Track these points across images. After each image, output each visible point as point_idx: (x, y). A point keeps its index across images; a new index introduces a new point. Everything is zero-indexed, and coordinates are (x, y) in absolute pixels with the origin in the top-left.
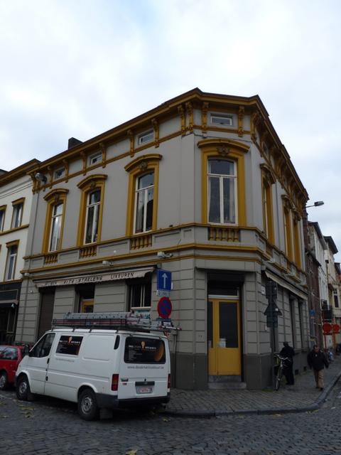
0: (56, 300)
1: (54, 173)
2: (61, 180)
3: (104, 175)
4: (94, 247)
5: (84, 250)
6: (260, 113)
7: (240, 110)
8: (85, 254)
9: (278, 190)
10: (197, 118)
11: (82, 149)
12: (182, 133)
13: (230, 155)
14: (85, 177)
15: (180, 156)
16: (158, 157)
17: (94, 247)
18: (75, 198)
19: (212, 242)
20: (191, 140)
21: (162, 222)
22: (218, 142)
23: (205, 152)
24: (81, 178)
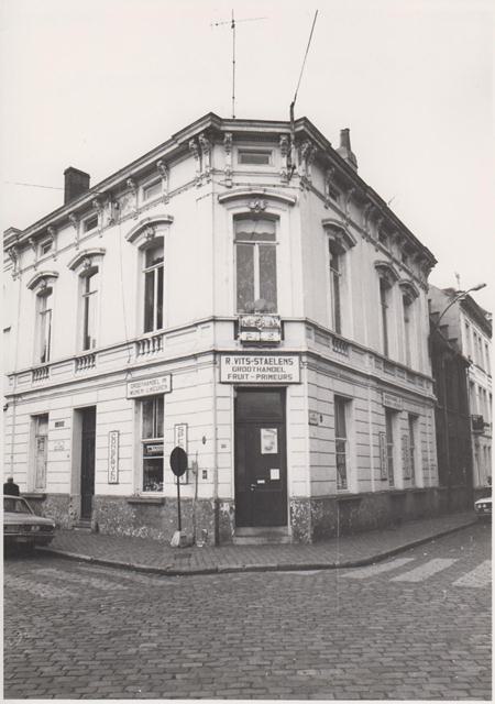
0: (97, 416)
1: (39, 247)
2: (154, 203)
3: (169, 217)
4: (92, 356)
5: (85, 360)
6: (314, 143)
7: (281, 142)
8: (141, 351)
9: (363, 257)
10: (222, 159)
11: (71, 210)
12: (197, 183)
13: (268, 210)
14: (138, 221)
15: (195, 218)
16: (166, 219)
17: (92, 356)
18: (67, 287)
19: (245, 350)
20: (216, 187)
21: (54, 358)
22: (249, 193)
23: (228, 209)
24: (73, 254)
